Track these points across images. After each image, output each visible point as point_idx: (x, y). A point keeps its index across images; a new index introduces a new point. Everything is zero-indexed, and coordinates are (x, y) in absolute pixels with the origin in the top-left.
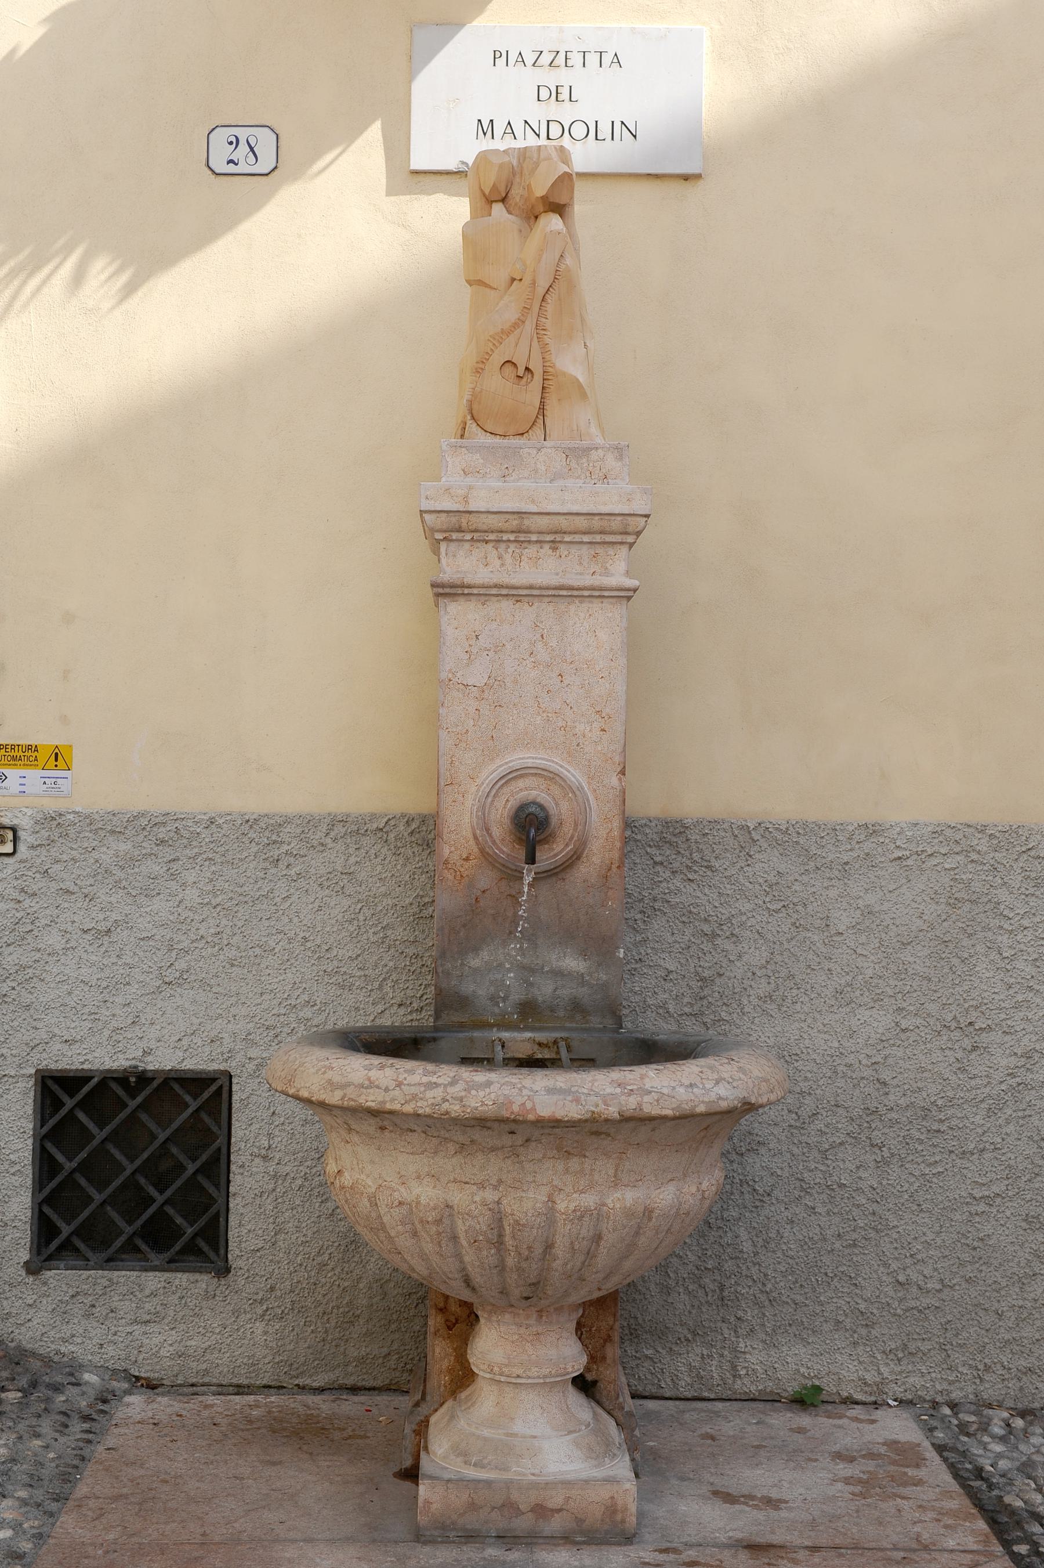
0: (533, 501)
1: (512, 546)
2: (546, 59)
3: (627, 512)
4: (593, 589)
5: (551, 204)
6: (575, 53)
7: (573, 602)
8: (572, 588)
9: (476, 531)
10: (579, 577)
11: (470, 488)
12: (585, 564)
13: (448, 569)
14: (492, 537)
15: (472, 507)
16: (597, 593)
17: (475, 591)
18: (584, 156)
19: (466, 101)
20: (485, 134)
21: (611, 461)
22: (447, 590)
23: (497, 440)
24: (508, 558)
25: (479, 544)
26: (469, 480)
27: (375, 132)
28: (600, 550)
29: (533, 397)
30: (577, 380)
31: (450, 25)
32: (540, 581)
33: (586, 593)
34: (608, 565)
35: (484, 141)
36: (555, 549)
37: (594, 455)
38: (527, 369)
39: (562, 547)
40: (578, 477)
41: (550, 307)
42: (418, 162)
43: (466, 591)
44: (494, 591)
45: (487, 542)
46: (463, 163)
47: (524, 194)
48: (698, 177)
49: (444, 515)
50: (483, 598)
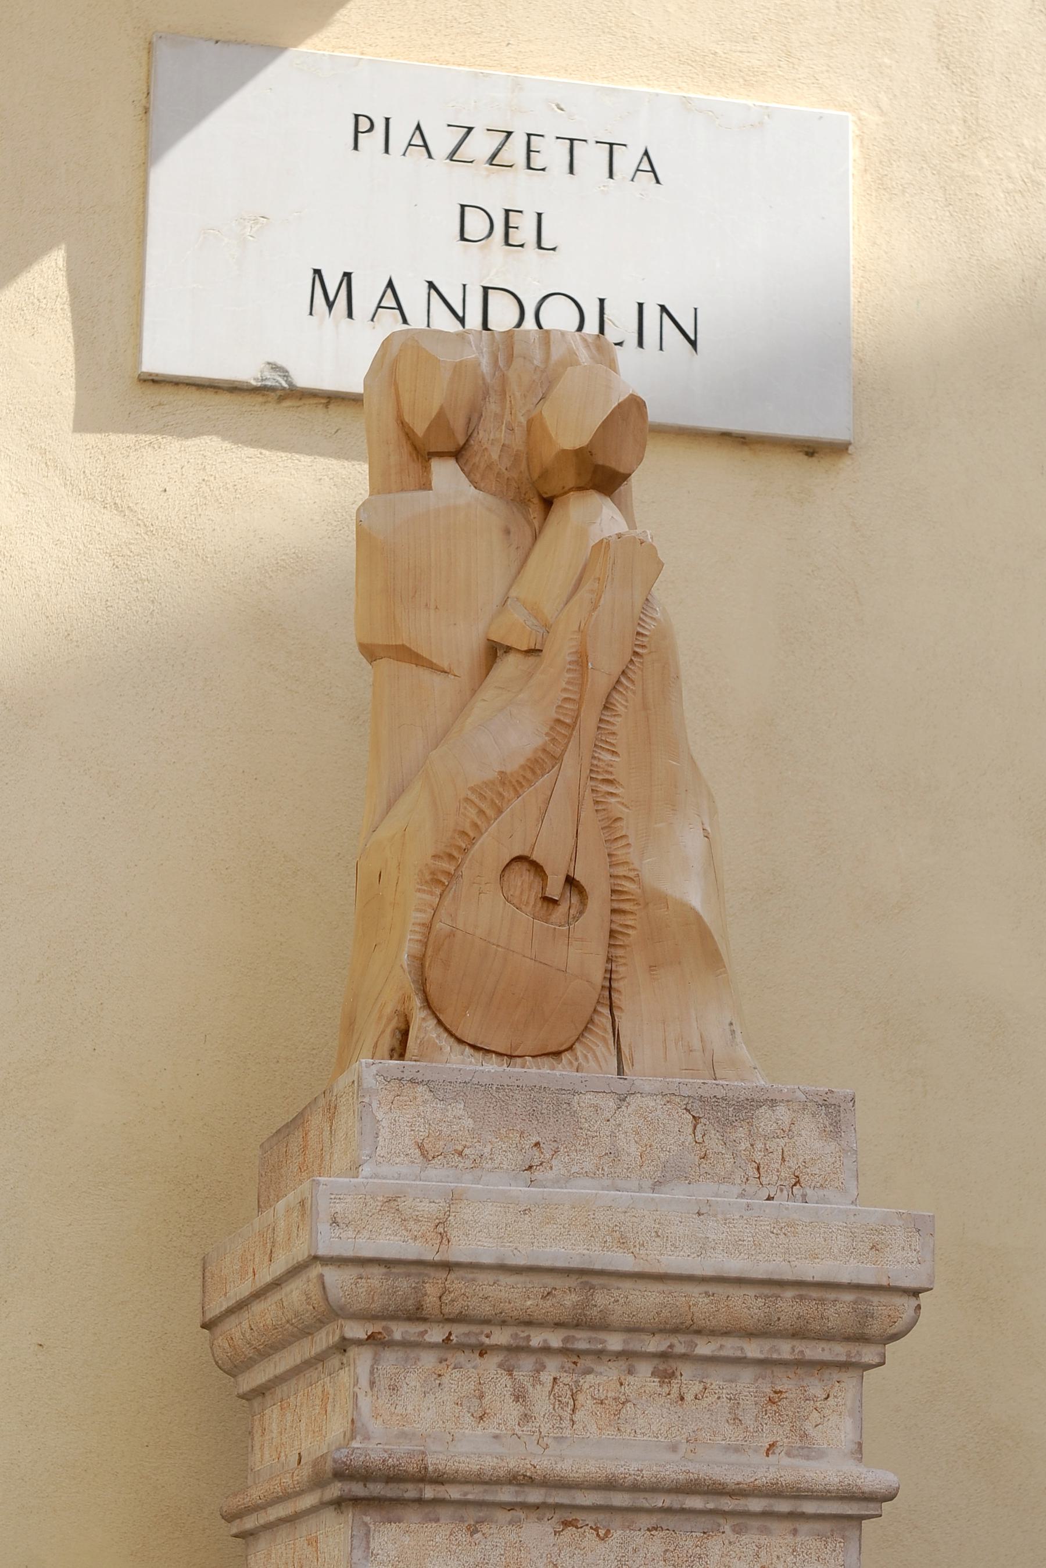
0: (622, 1242)
1: (553, 1366)
2: (480, 146)
3: (871, 1281)
4: (775, 1492)
5: (598, 469)
6: (550, 138)
7: (718, 1530)
8: (718, 1490)
9: (460, 1319)
10: (734, 1457)
11: (454, 1198)
12: (748, 1420)
13: (375, 1427)
14: (501, 1337)
15: (460, 1250)
16: (783, 1506)
17: (454, 1493)
18: (644, 372)
19: (286, 222)
20: (330, 305)
21: (809, 1139)
22: (377, 1489)
23: (492, 1067)
24: (541, 1399)
25: (461, 1357)
26: (438, 1176)
27: (49, 274)
28: (786, 1383)
29: (581, 952)
30: (699, 918)
31: (249, 47)
32: (633, 1467)
33: (756, 1505)
34: (808, 1426)
35: (329, 321)
36: (666, 1377)
37: (766, 1120)
38: (570, 881)
39: (687, 1370)
40: (724, 1180)
41: (621, 724)
42: (160, 357)
43: (429, 1492)
44: (506, 1495)
45: (483, 1351)
46: (275, 367)
47: (506, 445)
48: (838, 449)
49: (378, 1271)
50: (472, 1515)
